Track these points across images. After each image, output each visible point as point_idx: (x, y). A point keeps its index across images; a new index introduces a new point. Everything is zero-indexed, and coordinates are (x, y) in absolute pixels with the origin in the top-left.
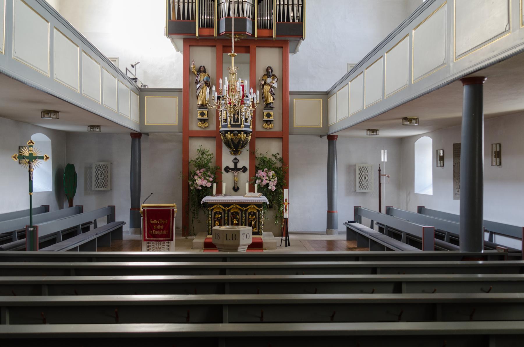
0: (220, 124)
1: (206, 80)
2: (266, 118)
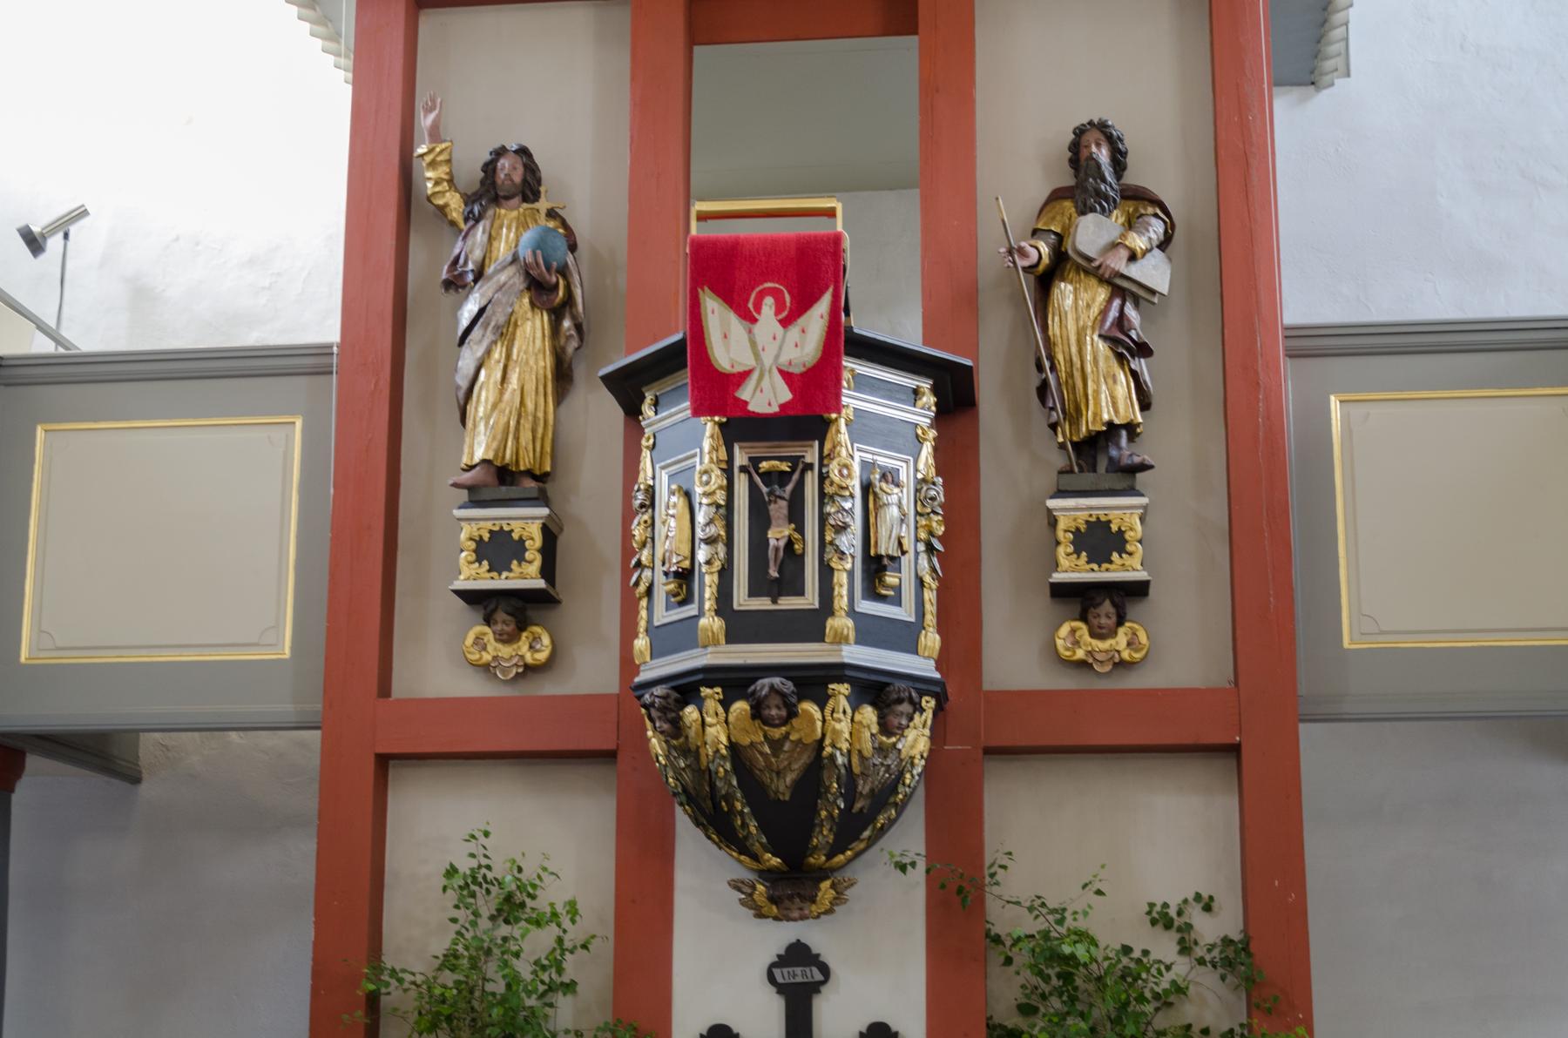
0: (643, 624)
1: (529, 252)
2: (1073, 569)
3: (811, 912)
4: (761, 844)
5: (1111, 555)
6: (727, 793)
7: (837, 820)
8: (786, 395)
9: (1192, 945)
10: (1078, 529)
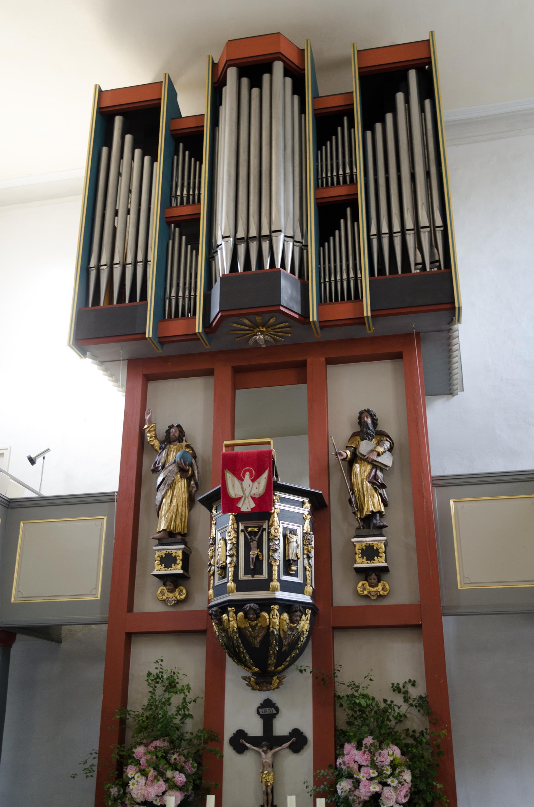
2: (362, 563)
3: (271, 688)
4: (251, 663)
5: (374, 557)
6: (237, 645)
7: (276, 654)
8: (253, 505)
9: (408, 699)
10: (363, 549)
